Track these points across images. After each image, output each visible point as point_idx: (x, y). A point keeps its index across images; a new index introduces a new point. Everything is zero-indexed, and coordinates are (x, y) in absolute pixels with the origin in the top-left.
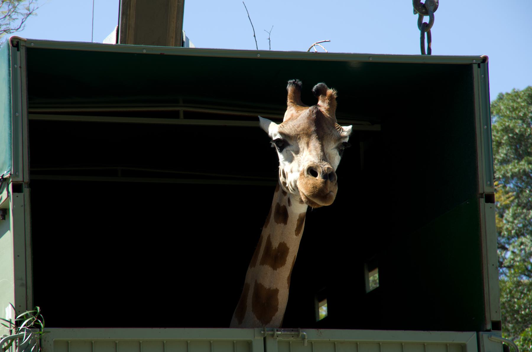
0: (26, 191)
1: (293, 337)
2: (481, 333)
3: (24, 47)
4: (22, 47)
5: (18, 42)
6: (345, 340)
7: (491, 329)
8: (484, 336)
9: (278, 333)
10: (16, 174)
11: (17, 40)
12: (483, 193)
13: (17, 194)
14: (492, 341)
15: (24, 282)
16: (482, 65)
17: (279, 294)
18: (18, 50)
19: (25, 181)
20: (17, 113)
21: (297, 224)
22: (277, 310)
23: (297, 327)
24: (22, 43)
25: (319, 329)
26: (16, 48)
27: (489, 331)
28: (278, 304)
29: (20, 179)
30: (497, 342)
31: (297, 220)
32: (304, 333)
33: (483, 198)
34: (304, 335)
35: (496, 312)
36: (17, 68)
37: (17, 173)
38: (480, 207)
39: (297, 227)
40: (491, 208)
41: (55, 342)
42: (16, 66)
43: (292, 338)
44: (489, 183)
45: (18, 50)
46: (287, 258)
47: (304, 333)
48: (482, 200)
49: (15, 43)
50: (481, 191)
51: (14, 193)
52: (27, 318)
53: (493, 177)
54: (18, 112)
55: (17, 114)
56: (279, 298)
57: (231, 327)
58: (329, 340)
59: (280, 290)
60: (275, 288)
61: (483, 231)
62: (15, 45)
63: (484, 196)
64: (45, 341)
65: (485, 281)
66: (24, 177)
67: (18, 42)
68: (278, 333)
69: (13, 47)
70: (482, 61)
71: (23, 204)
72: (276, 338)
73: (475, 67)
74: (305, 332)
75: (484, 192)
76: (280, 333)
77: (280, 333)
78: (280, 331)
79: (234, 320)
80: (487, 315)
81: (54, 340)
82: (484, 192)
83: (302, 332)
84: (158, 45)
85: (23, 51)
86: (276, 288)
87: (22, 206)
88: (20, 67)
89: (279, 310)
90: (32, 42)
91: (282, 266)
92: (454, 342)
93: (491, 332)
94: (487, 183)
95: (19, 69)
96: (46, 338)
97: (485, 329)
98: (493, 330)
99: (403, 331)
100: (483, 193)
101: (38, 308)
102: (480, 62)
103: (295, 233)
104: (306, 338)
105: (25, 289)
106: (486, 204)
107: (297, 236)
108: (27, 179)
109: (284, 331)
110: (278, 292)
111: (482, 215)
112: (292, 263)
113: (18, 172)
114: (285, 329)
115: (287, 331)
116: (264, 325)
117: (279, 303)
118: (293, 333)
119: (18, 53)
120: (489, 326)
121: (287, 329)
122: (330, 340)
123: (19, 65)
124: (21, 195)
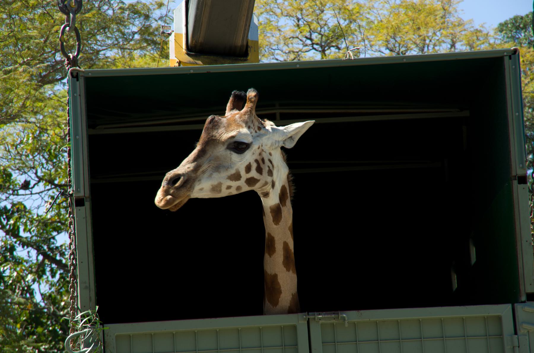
0: (88, 204)
1: (334, 319)
2: (516, 304)
3: (82, 77)
4: (81, 77)
5: (77, 73)
6: (385, 319)
7: (525, 300)
8: (519, 307)
9: (319, 317)
10: (77, 190)
11: (76, 72)
12: (516, 176)
13: (79, 208)
14: (526, 311)
15: (88, 285)
16: (513, 56)
17: (279, 278)
18: (78, 80)
19: (86, 195)
20: (77, 136)
21: (272, 215)
22: (280, 292)
23: (337, 310)
24: (81, 74)
25: (359, 311)
26: (75, 79)
27: (524, 302)
28: (280, 287)
29: (81, 194)
30: (532, 312)
31: (269, 212)
32: (344, 315)
33: (516, 180)
34: (344, 317)
35: (531, 284)
36: (76, 96)
37: (78, 189)
38: (513, 188)
39: (273, 218)
40: (524, 188)
41: (117, 337)
42: (75, 95)
43: (334, 321)
44: (521, 165)
45: (78, 80)
46: (276, 245)
47: (344, 315)
48: (515, 182)
49: (75, 74)
50: (514, 174)
51: (76, 207)
52: (87, 316)
53: (525, 160)
54: (78, 135)
55: (77, 137)
56: (279, 281)
57: (265, 315)
58: (369, 320)
59: (278, 274)
60: (274, 273)
61: (516, 210)
62: (75, 76)
63: (517, 178)
64: (107, 336)
65: (520, 256)
66: (84, 192)
67: (77, 73)
68: (319, 317)
69: (72, 78)
70: (513, 52)
71: (85, 216)
72: (319, 322)
73: (506, 59)
74: (345, 314)
75: (517, 175)
76: (321, 316)
77: (321, 316)
78: (321, 315)
79: (267, 304)
80: (522, 288)
81: (115, 334)
82: (517, 175)
83: (341, 314)
84: (211, 65)
85: (82, 80)
86: (275, 273)
87: (84, 218)
88: (80, 95)
89: (282, 291)
90: (89, 72)
91: (273, 253)
92: (490, 314)
93: (526, 303)
94: (519, 166)
95: (78, 97)
96: (108, 333)
97: (520, 301)
98: (527, 301)
99: (440, 308)
100: (516, 176)
101: (97, 307)
102: (510, 54)
103: (274, 224)
104: (346, 319)
105: (89, 291)
106: (518, 185)
107: (277, 225)
108: (88, 193)
109: (325, 314)
110: (277, 277)
111: (515, 195)
112: (283, 249)
113: (80, 188)
114: (327, 312)
115: (328, 314)
116: (275, 307)
117: (281, 286)
118: (333, 316)
119: (78, 83)
120: (524, 298)
121: (329, 312)
122: (371, 320)
123: (78, 93)
124: (82, 208)
